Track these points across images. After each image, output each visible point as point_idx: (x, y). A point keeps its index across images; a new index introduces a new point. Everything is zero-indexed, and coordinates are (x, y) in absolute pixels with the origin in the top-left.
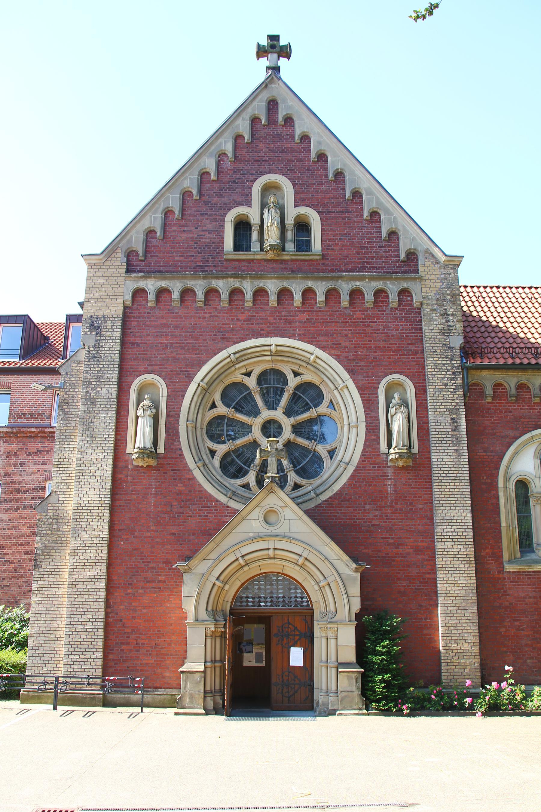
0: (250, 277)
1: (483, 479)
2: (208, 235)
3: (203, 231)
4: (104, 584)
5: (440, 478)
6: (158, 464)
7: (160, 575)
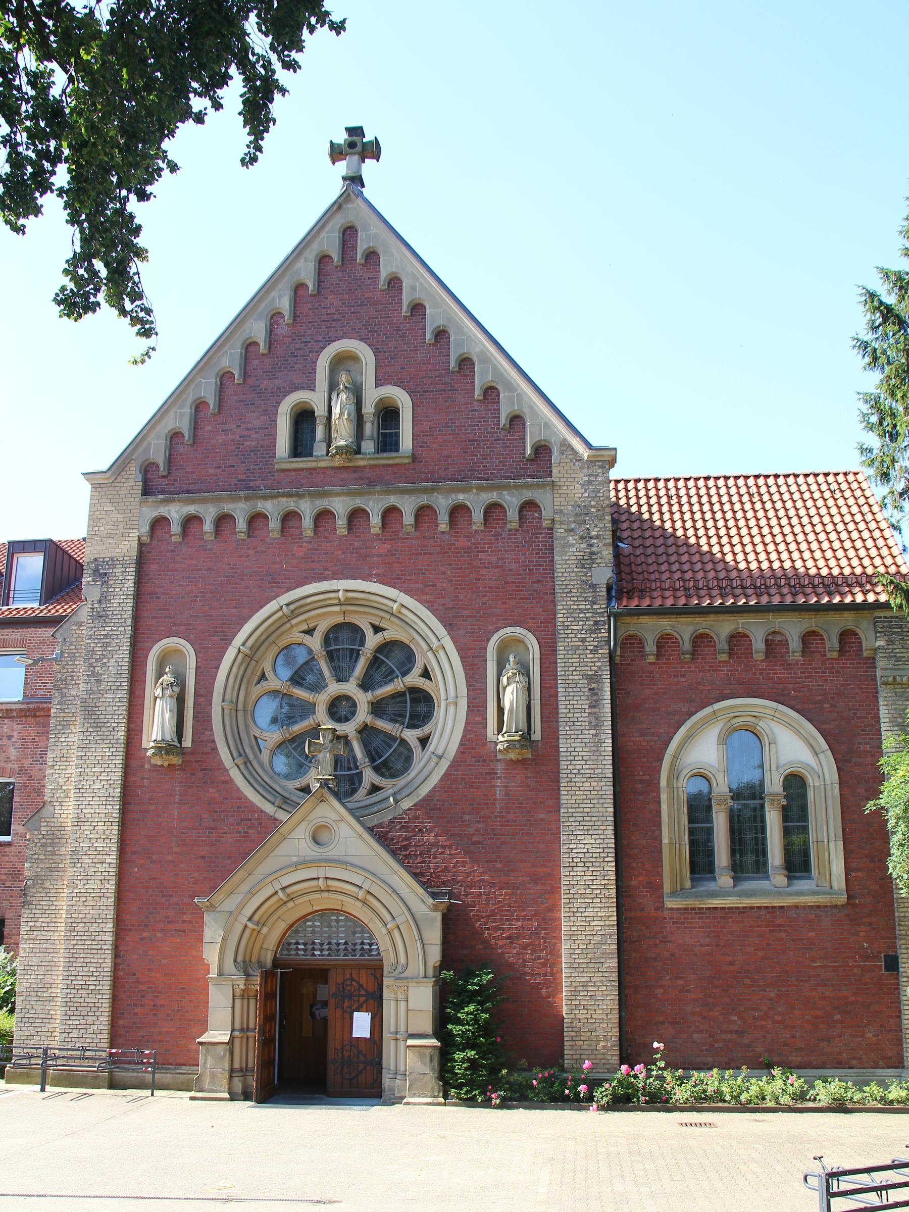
0: (309, 495)
1: (638, 775)
2: (254, 436)
3: (247, 429)
4: (111, 925)
5: (570, 776)
6: (183, 762)
7: (185, 913)
